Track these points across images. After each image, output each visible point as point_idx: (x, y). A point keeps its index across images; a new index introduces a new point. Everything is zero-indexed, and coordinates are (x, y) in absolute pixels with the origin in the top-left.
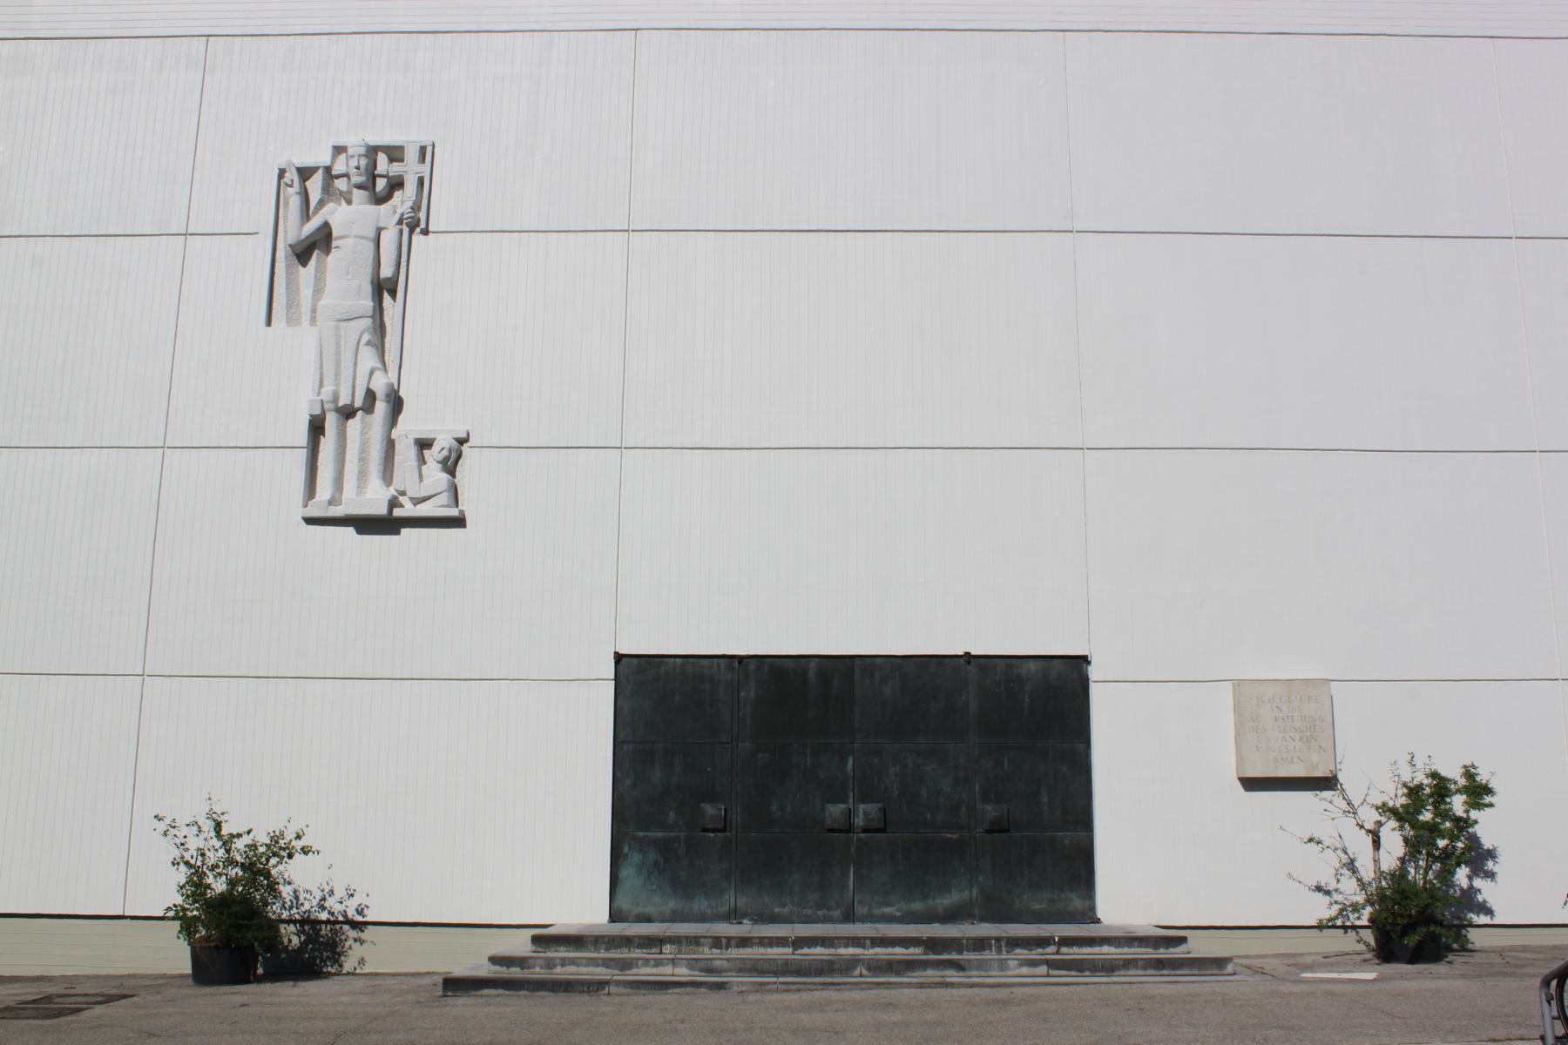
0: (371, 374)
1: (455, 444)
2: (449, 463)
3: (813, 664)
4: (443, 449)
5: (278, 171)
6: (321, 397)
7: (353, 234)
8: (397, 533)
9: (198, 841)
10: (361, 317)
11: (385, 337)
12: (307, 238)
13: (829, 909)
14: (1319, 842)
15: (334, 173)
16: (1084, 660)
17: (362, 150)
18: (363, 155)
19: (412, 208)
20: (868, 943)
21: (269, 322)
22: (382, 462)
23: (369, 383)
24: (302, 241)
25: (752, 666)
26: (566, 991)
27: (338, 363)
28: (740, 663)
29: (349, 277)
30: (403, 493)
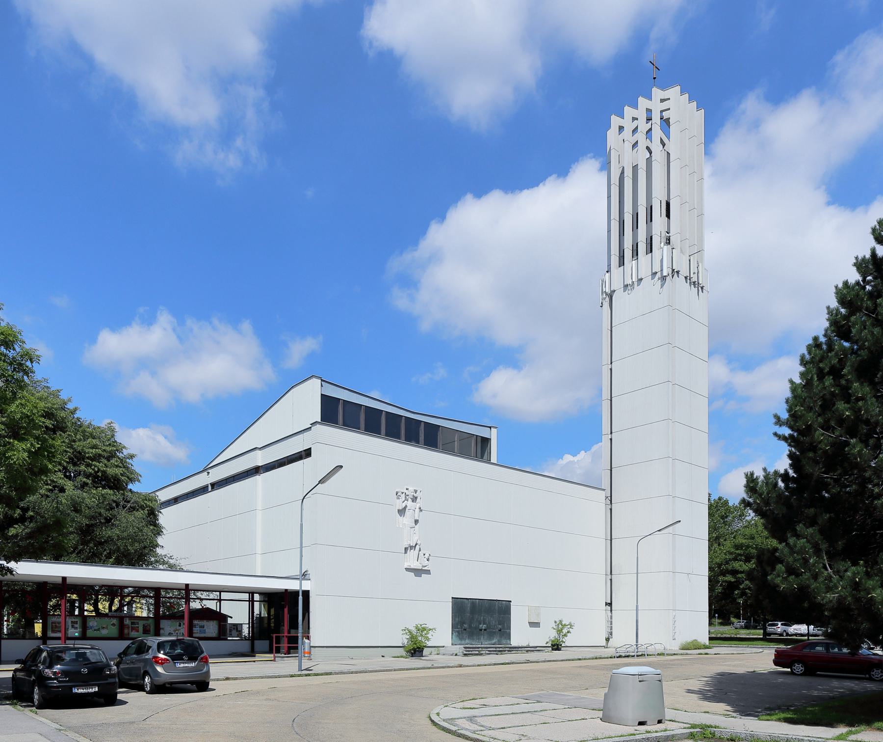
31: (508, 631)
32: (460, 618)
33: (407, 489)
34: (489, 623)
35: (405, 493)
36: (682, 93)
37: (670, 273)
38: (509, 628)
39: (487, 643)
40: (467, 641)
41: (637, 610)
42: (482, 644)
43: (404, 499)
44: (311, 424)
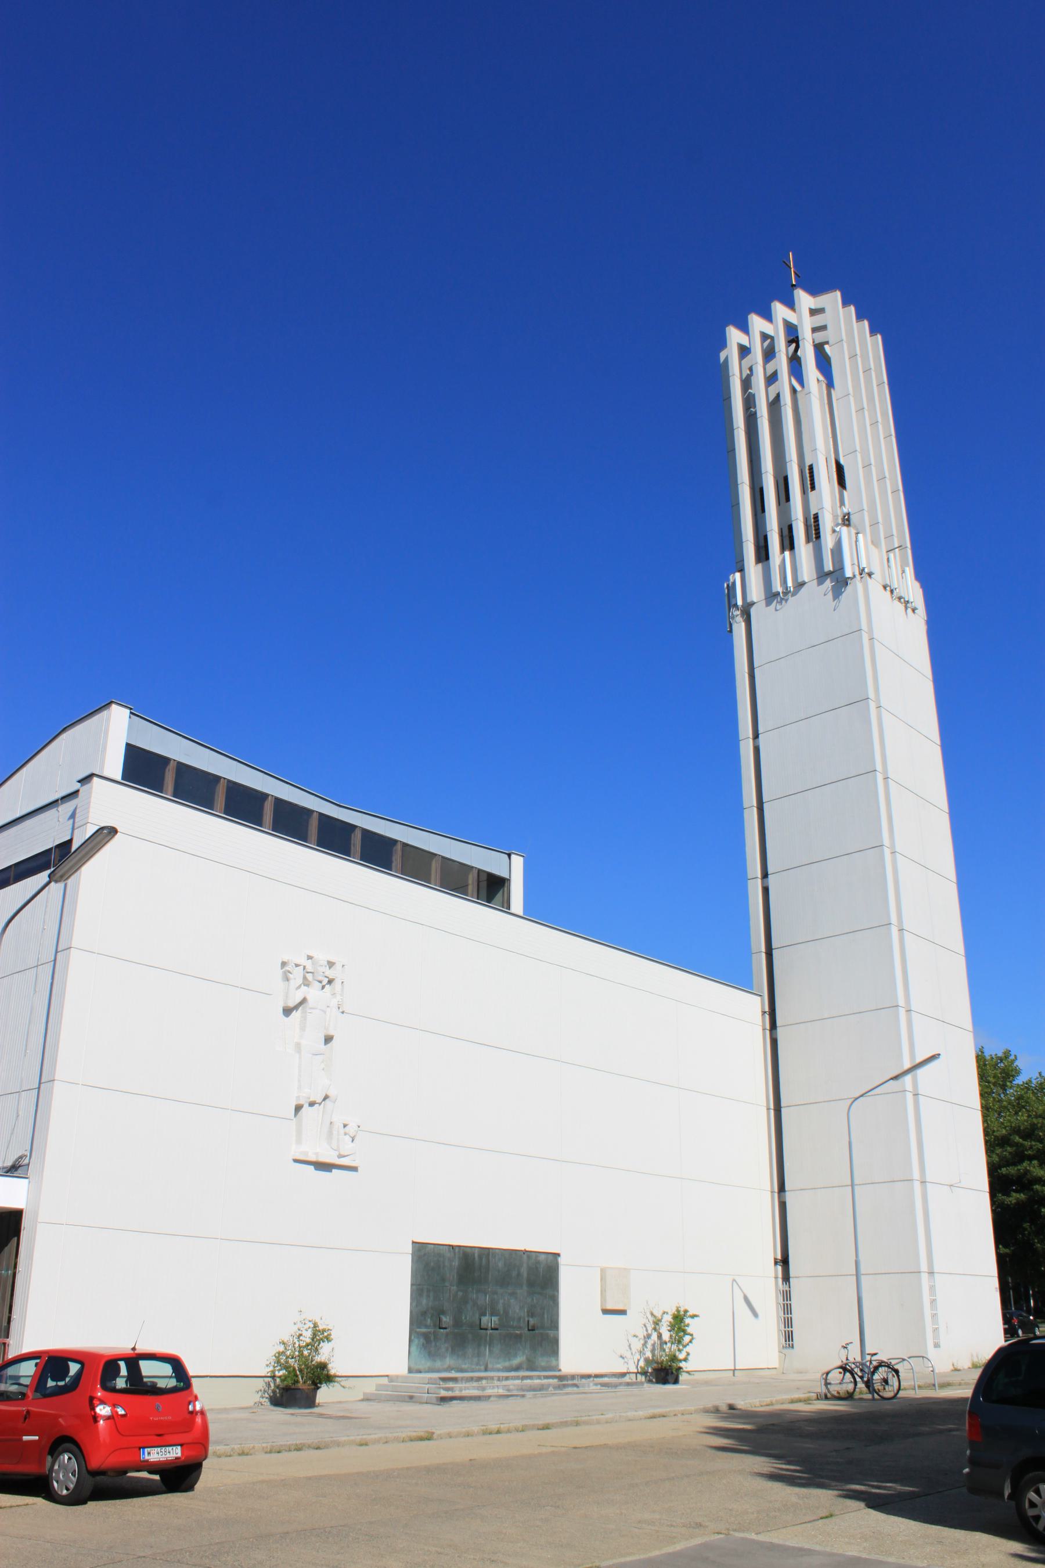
3: (477, 1250)
8: (331, 1171)
13: (480, 1366)
14: (637, 1337)
16: (558, 1255)
20: (542, 1378)
25: (457, 1251)
26: (479, 1400)
28: (453, 1248)
31: (551, 1333)
32: (431, 1298)
33: (310, 958)
34: (506, 1312)
35: (304, 968)
36: (846, 303)
37: (857, 573)
38: (555, 1325)
39: (499, 1366)
40: (449, 1361)
41: (858, 1275)
42: (486, 1370)
43: (300, 981)
44: (79, 782)
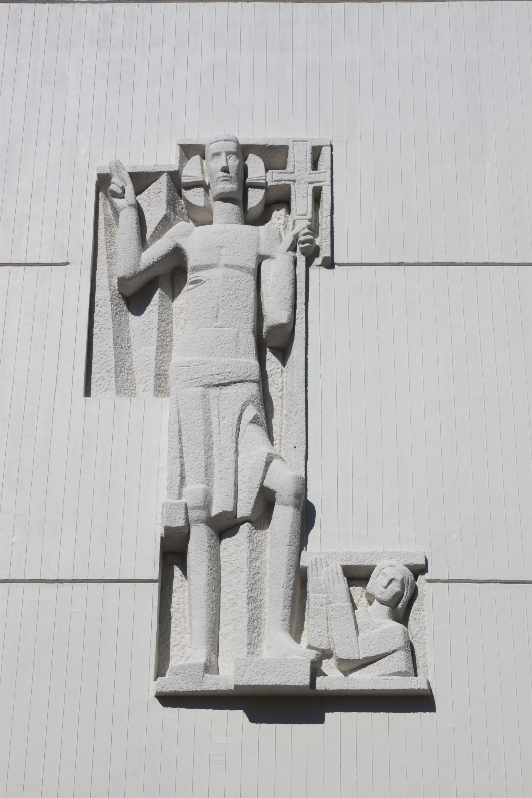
0: (268, 463)
1: (409, 575)
2: (400, 605)
4: (390, 582)
5: (95, 178)
6: (183, 500)
7: (223, 262)
8: (321, 720)
9: (387, 617)
10: (242, 381)
11: (272, 417)
12: (148, 268)
15: (184, 180)
17: (232, 147)
18: (234, 153)
19: (309, 227)
21: (87, 392)
22: (288, 603)
23: (264, 477)
24: (141, 273)
27: (209, 449)
29: (220, 323)
30: (327, 654)
